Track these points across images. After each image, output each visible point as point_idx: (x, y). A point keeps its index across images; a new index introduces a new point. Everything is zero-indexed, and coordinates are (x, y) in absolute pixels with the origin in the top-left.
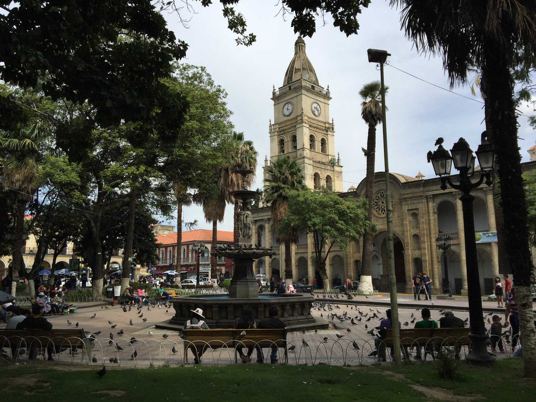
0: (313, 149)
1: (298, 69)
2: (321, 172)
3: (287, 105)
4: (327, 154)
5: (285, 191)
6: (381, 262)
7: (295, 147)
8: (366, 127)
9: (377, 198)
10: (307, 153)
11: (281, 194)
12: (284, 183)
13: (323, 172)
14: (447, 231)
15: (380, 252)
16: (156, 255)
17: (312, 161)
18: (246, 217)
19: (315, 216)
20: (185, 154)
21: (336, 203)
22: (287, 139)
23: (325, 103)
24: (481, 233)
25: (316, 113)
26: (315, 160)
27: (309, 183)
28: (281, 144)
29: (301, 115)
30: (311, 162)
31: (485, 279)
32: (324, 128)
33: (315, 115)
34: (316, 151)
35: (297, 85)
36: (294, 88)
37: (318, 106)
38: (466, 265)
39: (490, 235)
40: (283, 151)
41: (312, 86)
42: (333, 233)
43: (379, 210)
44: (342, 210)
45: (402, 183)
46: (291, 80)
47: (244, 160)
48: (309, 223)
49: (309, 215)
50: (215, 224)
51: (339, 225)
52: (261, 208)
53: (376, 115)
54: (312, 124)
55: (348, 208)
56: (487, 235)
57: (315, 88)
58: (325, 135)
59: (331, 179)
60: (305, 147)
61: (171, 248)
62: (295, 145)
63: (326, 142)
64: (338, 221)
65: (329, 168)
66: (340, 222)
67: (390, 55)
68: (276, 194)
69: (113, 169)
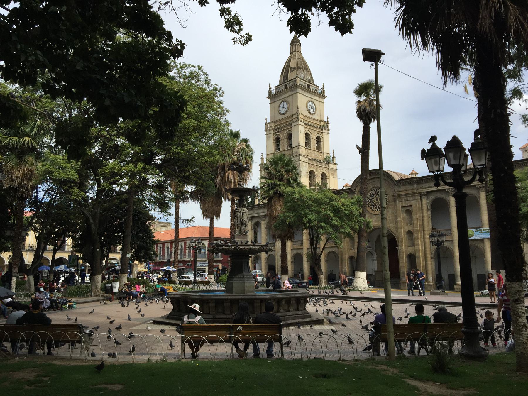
0: (308, 147)
1: (294, 68)
2: (316, 169)
3: (282, 103)
4: (322, 151)
5: (280, 188)
6: (375, 258)
7: (291, 145)
8: (360, 125)
9: (372, 195)
10: (302, 150)
11: (277, 191)
12: (280, 180)
13: (318, 170)
14: (441, 228)
15: (375, 249)
16: (154, 252)
17: (307, 159)
18: (243, 214)
19: (310, 213)
20: (182, 152)
21: (331, 200)
22: (283, 137)
23: (320, 102)
24: (474, 230)
25: (312, 111)
26: (310, 157)
27: (305, 180)
28: (277, 142)
29: (297, 113)
30: (306, 160)
31: (478, 275)
32: (319, 126)
33: (310, 113)
34: (312, 148)
35: (293, 84)
36: (290, 87)
37: (313, 105)
39: (483, 231)
40: (279, 149)
41: (308, 85)
42: (328, 229)
43: (374, 207)
44: (336, 207)
45: (396, 181)
46: (287, 78)
47: (241, 158)
48: (304, 219)
49: (304, 211)
50: (212, 221)
51: (334, 222)
52: (257, 205)
53: (370, 113)
54: (307, 122)
55: (343, 205)
56: (480, 231)
57: (311, 87)
58: (320, 133)
59: (326, 176)
60: (300, 144)
61: (169, 244)
62: (290, 143)
63: (321, 140)
64: (333, 218)
65: (324, 165)
66: (335, 219)
67: (384, 54)
68: (272, 191)
69: (111, 167)
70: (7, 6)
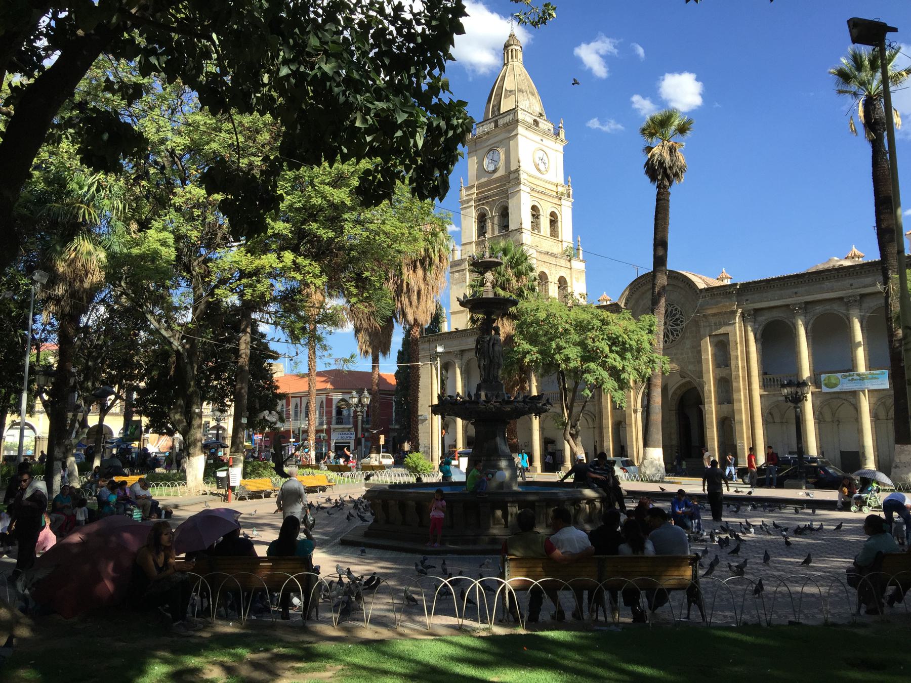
0: (536, 232)
1: (510, 91)
2: (550, 270)
4: (560, 239)
7: (506, 227)
8: (652, 190)
13: (553, 271)
14: (724, 372)
18: (493, 344)
22: (493, 214)
24: (839, 375)
25: (542, 167)
26: (540, 249)
28: (481, 222)
29: (517, 171)
31: (841, 452)
32: (555, 194)
33: (539, 170)
34: (542, 233)
35: (509, 118)
36: (504, 125)
39: (855, 377)
41: (535, 121)
45: (701, 290)
46: (499, 109)
47: (431, 251)
48: (557, 357)
50: (375, 360)
53: (671, 168)
54: (534, 187)
55: (626, 331)
56: (850, 378)
57: (540, 125)
58: (556, 206)
59: (566, 282)
63: (557, 218)
64: (609, 355)
67: (895, 30)
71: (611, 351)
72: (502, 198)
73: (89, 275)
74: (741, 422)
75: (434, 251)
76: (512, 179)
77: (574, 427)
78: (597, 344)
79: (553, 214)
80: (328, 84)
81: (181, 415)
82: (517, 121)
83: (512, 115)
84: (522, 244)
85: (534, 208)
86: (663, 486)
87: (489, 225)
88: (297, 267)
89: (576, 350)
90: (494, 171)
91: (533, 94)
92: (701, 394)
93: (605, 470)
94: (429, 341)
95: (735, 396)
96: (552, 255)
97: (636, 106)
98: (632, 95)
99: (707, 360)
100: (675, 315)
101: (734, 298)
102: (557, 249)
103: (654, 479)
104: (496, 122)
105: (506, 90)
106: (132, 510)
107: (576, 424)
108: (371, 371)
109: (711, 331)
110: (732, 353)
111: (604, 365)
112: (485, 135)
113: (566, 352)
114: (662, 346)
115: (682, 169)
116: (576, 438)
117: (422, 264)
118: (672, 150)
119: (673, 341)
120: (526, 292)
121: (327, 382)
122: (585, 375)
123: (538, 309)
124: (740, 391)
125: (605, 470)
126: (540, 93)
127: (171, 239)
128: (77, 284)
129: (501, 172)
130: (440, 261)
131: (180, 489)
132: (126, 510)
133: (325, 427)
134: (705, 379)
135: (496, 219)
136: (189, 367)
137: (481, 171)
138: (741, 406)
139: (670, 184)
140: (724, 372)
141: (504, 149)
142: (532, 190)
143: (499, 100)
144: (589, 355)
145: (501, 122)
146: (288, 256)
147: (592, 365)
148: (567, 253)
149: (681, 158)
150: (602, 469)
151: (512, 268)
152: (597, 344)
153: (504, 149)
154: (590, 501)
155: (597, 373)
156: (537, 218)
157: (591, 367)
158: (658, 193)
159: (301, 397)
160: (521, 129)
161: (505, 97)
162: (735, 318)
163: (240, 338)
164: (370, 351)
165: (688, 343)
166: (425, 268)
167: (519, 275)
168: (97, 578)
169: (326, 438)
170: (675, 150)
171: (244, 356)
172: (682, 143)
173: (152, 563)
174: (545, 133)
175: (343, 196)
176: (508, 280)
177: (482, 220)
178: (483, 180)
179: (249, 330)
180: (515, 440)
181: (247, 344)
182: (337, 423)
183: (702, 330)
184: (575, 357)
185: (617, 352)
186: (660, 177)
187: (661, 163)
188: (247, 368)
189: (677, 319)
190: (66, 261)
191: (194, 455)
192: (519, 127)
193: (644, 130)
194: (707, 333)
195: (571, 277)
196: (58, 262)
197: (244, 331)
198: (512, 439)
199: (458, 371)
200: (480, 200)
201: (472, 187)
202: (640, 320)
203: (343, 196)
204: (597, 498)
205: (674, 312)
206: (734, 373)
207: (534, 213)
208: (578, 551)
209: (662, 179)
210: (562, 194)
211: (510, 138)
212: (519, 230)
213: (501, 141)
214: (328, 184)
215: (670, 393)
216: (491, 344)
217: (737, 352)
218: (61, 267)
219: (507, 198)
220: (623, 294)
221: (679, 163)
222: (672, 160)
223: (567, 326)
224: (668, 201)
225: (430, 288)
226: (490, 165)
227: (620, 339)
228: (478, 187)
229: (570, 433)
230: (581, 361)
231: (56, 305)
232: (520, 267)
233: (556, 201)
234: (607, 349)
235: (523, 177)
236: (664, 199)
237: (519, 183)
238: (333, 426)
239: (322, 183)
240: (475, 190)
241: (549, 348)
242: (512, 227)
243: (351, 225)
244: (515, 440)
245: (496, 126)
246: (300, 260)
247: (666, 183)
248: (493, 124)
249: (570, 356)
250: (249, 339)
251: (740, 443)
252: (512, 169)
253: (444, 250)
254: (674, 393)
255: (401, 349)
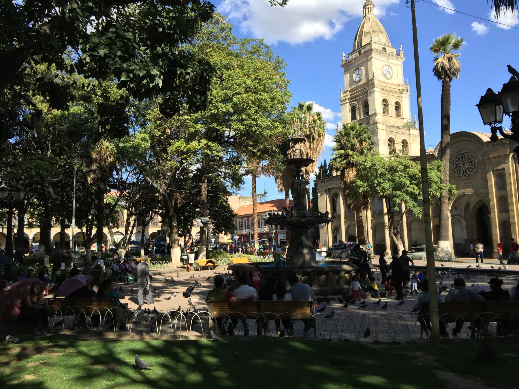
1: (368, 32)
2: (395, 136)
3: (357, 70)
5: (353, 158)
6: (465, 226)
7: (367, 113)
9: (458, 160)
10: (380, 118)
11: (350, 161)
12: (353, 150)
14: (503, 193)
15: (463, 216)
16: (233, 225)
17: (384, 126)
18: (300, 185)
19: (384, 182)
20: (242, 127)
21: (406, 167)
22: (360, 106)
23: (397, 65)
25: (388, 76)
27: (383, 150)
28: (353, 111)
29: (372, 79)
30: (384, 127)
33: (387, 78)
36: (364, 53)
37: (390, 68)
38: (341, 209)
40: (355, 118)
41: (383, 48)
42: (404, 198)
43: (460, 172)
44: (413, 173)
46: (361, 44)
47: (313, 131)
48: (378, 188)
49: (377, 180)
51: (410, 190)
52: (335, 176)
53: (449, 70)
59: (407, 143)
60: (377, 112)
61: (246, 218)
62: (367, 111)
64: (410, 186)
65: (403, 131)
66: (412, 186)
68: (345, 161)
69: (178, 146)
70: (504, 114)
71: (411, 183)
72: (364, 96)
73: (109, 158)
74: (515, 223)
75: (314, 131)
76: (370, 84)
77: (396, 229)
78: (401, 179)
79: (397, 103)
80: (107, 60)
81: (168, 227)
82: (372, 50)
83: (369, 47)
84: (377, 123)
85: (384, 100)
86: (443, 263)
87: (357, 112)
88: (209, 147)
89: (389, 184)
90: (359, 81)
91: (382, 33)
92: (488, 207)
93: (359, 254)
94: (324, 182)
95: (510, 208)
96: (397, 127)
97: (475, 29)
98: (472, 22)
99: (492, 185)
100: (470, 159)
101: (508, 146)
102: (399, 122)
103: (444, 260)
104: (360, 52)
105: (365, 32)
106: (128, 276)
107: (397, 228)
108: (284, 198)
109: (494, 168)
110: (508, 181)
111: (407, 193)
112: (353, 60)
113: (383, 185)
114: (448, 179)
115: (458, 70)
116: (397, 236)
117: (308, 139)
118: (450, 59)
119: (469, 175)
120: (365, 152)
121: (274, 206)
122: (394, 199)
123: (365, 161)
124: (513, 204)
125: (359, 254)
126: (386, 31)
127: (147, 136)
128: (103, 163)
129: (363, 81)
130: (319, 136)
131: (169, 264)
132: (125, 275)
133: (274, 231)
134: (490, 197)
135: (361, 109)
136: (169, 202)
137: (352, 82)
138: (514, 214)
139: (450, 81)
140: (503, 193)
141: (365, 67)
142: (383, 90)
143: (361, 38)
144: (398, 187)
145: (362, 51)
146: (204, 142)
147: (399, 192)
148: (408, 125)
149: (456, 63)
150: (358, 254)
151: (357, 138)
152: (401, 179)
153: (365, 67)
154: (348, 272)
155: (402, 197)
156: (387, 106)
157: (398, 194)
158: (443, 86)
159: (261, 215)
160: (374, 55)
161: (365, 36)
162: (508, 159)
163: (201, 186)
164: (283, 189)
165: (479, 176)
166: (310, 141)
167: (361, 142)
168: (12, 307)
169: (275, 237)
170: (452, 59)
171: (204, 195)
172: (459, 52)
173: (30, 300)
174: (391, 55)
175: (229, 107)
176: (354, 145)
177: (353, 110)
178: (353, 87)
179: (206, 181)
180: (363, 237)
181: (205, 188)
182: (281, 229)
183: (487, 167)
184: (389, 188)
185: (415, 184)
186: (443, 76)
187: (443, 68)
188: (206, 201)
189: (472, 162)
190: (96, 152)
191: (174, 247)
192: (373, 54)
193: (431, 48)
194: (491, 169)
195: (410, 140)
196: (93, 153)
197: (204, 182)
198: (361, 237)
199: (341, 198)
200: (352, 99)
201: (347, 91)
202: (431, 164)
203: (229, 107)
204: (353, 270)
205: (469, 157)
206: (509, 193)
207: (385, 103)
208: (246, 298)
209: (445, 78)
210: (403, 90)
211: (368, 61)
212: (375, 114)
213: (362, 63)
214: (221, 102)
215: (471, 206)
216: (299, 184)
217: (511, 180)
218: (94, 155)
219: (367, 96)
220: (436, 148)
221: (455, 67)
222: (450, 65)
223: (384, 170)
224: (449, 90)
225: (314, 152)
226: (357, 78)
227: (417, 176)
228: (350, 92)
229: (393, 233)
230: (392, 190)
231: (94, 174)
232: (362, 137)
233: (399, 95)
234: (408, 182)
235: (376, 82)
236: (446, 90)
237: (374, 87)
238: (279, 231)
239: (217, 101)
240: (348, 93)
241: (374, 183)
242: (370, 113)
243: (235, 123)
244: (363, 237)
245: (360, 54)
246: (210, 143)
247: (448, 80)
248: (358, 54)
249: (386, 187)
250: (206, 186)
251: (514, 237)
252: (370, 79)
253: (320, 130)
254: (474, 207)
255: (314, 187)
